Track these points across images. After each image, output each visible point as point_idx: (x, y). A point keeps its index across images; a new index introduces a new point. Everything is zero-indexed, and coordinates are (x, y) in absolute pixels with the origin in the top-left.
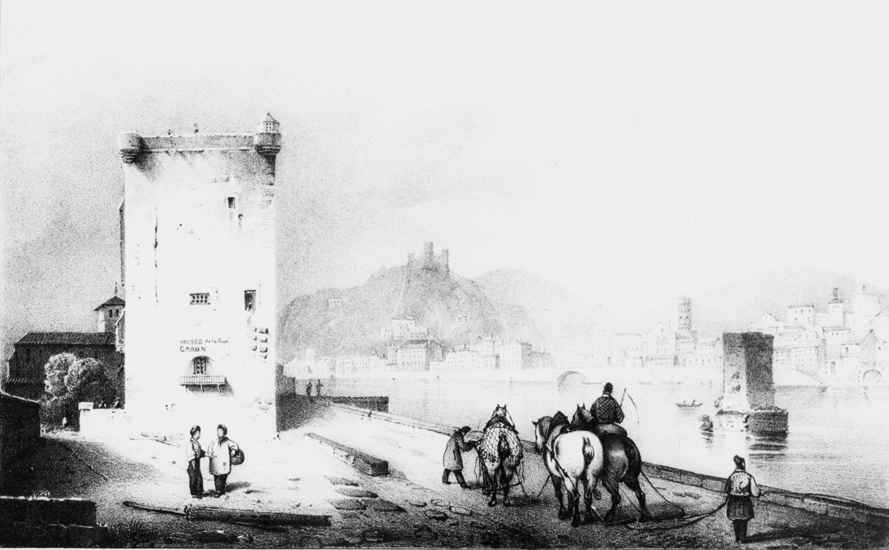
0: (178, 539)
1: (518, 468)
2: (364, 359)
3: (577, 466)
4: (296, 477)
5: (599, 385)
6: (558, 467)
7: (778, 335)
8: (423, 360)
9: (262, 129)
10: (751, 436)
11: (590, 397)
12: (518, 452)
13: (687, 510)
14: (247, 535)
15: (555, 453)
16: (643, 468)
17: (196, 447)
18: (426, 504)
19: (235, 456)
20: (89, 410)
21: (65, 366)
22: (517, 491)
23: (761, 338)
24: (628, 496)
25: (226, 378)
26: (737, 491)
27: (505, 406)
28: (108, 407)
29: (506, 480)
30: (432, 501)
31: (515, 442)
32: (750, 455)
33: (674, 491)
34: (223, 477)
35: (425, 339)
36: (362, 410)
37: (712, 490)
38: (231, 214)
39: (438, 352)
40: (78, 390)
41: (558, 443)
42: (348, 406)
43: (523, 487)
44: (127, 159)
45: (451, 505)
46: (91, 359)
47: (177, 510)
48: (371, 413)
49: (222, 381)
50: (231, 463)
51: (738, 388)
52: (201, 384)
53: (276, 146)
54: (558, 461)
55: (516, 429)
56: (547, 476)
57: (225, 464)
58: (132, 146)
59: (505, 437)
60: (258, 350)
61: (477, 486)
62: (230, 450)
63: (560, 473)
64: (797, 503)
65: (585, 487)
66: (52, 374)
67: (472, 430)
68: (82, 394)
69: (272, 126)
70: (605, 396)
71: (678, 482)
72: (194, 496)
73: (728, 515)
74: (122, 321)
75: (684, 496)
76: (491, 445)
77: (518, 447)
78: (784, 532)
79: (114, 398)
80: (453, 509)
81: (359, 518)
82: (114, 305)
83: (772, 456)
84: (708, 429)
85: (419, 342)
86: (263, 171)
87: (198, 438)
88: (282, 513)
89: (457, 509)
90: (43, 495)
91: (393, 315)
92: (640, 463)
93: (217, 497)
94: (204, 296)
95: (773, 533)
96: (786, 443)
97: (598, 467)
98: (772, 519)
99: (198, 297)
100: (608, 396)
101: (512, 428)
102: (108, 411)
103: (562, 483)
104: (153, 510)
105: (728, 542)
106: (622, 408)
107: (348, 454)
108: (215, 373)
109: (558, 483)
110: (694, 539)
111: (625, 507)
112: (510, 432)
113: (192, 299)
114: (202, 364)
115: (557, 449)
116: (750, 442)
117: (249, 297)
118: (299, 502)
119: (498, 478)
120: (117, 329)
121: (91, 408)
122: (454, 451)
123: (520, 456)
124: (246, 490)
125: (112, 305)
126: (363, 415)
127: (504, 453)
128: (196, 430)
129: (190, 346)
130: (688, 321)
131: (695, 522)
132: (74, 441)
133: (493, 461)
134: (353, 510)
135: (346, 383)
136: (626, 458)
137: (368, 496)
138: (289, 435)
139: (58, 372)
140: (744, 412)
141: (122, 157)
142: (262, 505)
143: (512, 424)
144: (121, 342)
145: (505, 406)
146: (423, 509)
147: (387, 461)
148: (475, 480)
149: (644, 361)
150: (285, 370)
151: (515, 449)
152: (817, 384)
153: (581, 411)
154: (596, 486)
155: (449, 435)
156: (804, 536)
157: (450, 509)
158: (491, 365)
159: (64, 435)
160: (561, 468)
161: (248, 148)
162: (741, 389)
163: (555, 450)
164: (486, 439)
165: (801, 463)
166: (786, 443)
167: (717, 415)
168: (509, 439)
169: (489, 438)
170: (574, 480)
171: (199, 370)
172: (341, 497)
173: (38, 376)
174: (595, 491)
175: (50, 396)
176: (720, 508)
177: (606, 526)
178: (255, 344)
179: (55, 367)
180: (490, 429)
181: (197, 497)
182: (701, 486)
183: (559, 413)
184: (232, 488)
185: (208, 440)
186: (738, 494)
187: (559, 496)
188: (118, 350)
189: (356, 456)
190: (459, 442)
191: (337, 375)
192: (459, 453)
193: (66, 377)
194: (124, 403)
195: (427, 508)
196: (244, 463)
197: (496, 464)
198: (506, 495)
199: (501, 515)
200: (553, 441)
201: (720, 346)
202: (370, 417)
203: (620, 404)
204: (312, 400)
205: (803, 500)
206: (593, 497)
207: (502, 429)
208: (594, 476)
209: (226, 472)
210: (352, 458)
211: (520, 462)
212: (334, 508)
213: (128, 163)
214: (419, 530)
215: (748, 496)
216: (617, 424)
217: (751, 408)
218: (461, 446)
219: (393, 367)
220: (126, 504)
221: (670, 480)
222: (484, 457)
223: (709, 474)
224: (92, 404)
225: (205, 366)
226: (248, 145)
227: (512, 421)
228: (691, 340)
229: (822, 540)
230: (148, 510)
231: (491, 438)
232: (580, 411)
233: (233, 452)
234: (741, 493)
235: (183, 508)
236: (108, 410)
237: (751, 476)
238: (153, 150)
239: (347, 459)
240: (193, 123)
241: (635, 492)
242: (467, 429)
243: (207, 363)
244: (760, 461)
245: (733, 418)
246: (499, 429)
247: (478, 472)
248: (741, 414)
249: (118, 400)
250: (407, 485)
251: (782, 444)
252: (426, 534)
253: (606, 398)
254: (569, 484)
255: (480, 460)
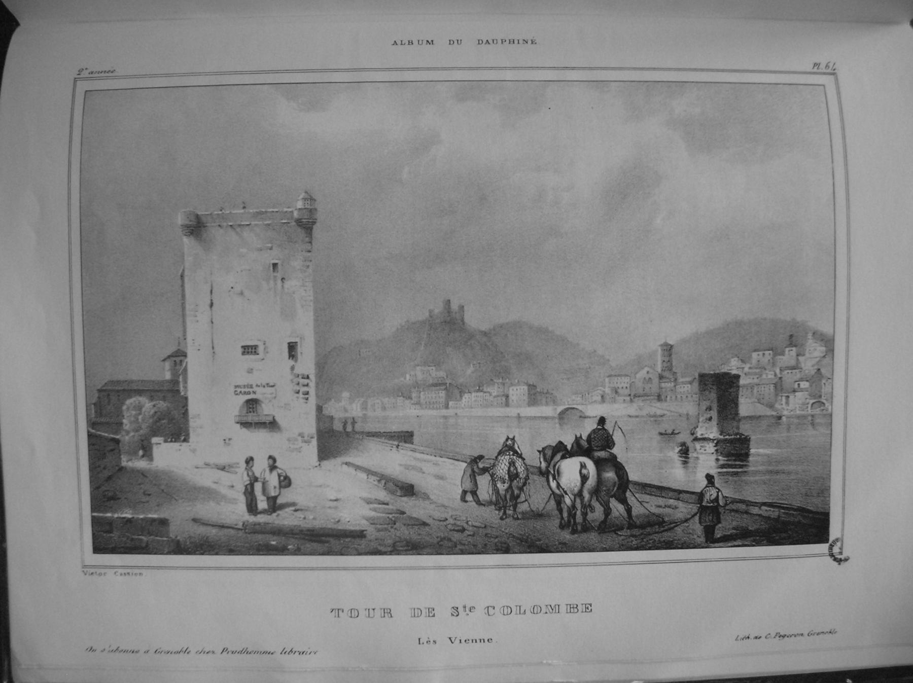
0: (238, 548)
1: (525, 488)
6: (559, 486)
7: (744, 375)
8: (443, 400)
12: (524, 476)
13: (666, 519)
14: (296, 545)
15: (557, 475)
17: (250, 474)
19: (283, 481)
20: (160, 444)
21: (139, 408)
22: (523, 507)
24: (617, 508)
27: (514, 437)
28: (175, 441)
30: (452, 516)
31: (522, 467)
32: (719, 473)
33: (656, 504)
34: (275, 498)
36: (391, 442)
37: (687, 502)
39: (456, 391)
42: (379, 440)
43: (529, 503)
44: (186, 233)
46: (161, 402)
48: (399, 445)
51: (710, 419)
55: (523, 456)
56: (549, 495)
57: (275, 487)
58: (191, 221)
61: (490, 503)
62: (279, 476)
63: (560, 491)
66: (128, 414)
67: (486, 457)
68: (155, 432)
69: (309, 202)
70: (599, 427)
71: (659, 497)
73: (700, 523)
74: (185, 370)
75: (664, 508)
76: (502, 469)
77: (525, 471)
79: (181, 434)
80: (470, 523)
81: (390, 532)
82: (178, 356)
83: (736, 474)
87: (252, 467)
89: (473, 522)
90: (126, 513)
93: (269, 515)
94: (254, 348)
95: (736, 535)
96: (748, 462)
98: (734, 524)
100: (601, 427)
101: (520, 456)
103: (562, 499)
105: (699, 542)
110: (672, 541)
111: (615, 518)
113: (243, 350)
114: (253, 405)
116: (720, 462)
119: (508, 497)
120: (181, 377)
121: (161, 442)
123: (527, 478)
124: (293, 508)
125: (176, 356)
126: (392, 447)
127: (513, 476)
129: (243, 390)
130: (669, 364)
131: (673, 528)
133: (504, 483)
134: (385, 525)
135: (377, 420)
136: (616, 478)
137: (398, 513)
138: (327, 464)
140: (715, 438)
141: (182, 231)
143: (520, 452)
144: (185, 388)
145: (514, 437)
146: (445, 523)
147: (413, 484)
148: (488, 499)
149: (632, 398)
153: (579, 440)
154: (591, 501)
155: (466, 462)
157: (467, 523)
158: (502, 403)
160: (561, 487)
161: (289, 221)
163: (556, 473)
164: (498, 465)
165: (760, 478)
166: (748, 462)
168: (517, 465)
169: (500, 464)
170: (572, 497)
171: (251, 410)
172: (373, 514)
174: (590, 506)
175: (128, 432)
176: (693, 516)
177: (599, 533)
180: (501, 457)
182: (678, 499)
184: (283, 507)
185: (260, 467)
186: (708, 505)
187: (560, 511)
188: (182, 394)
191: (370, 413)
192: (475, 476)
195: (448, 522)
197: (506, 485)
198: (515, 510)
200: (555, 466)
202: (398, 448)
203: (611, 433)
204: (348, 434)
205: (760, 508)
206: (588, 510)
207: (512, 456)
209: (276, 494)
210: (383, 482)
214: (441, 541)
216: (609, 450)
217: (721, 435)
220: (195, 520)
221: (653, 495)
222: (496, 480)
224: (162, 438)
225: (256, 406)
227: (520, 450)
230: (213, 526)
231: (502, 464)
232: (578, 440)
233: (282, 478)
234: (710, 503)
236: (176, 444)
239: (379, 483)
241: (624, 505)
242: (481, 457)
243: (258, 405)
246: (508, 456)
247: (491, 492)
248: (712, 439)
249: (184, 435)
250: (430, 503)
252: (446, 543)
253: (600, 429)
254: (568, 500)
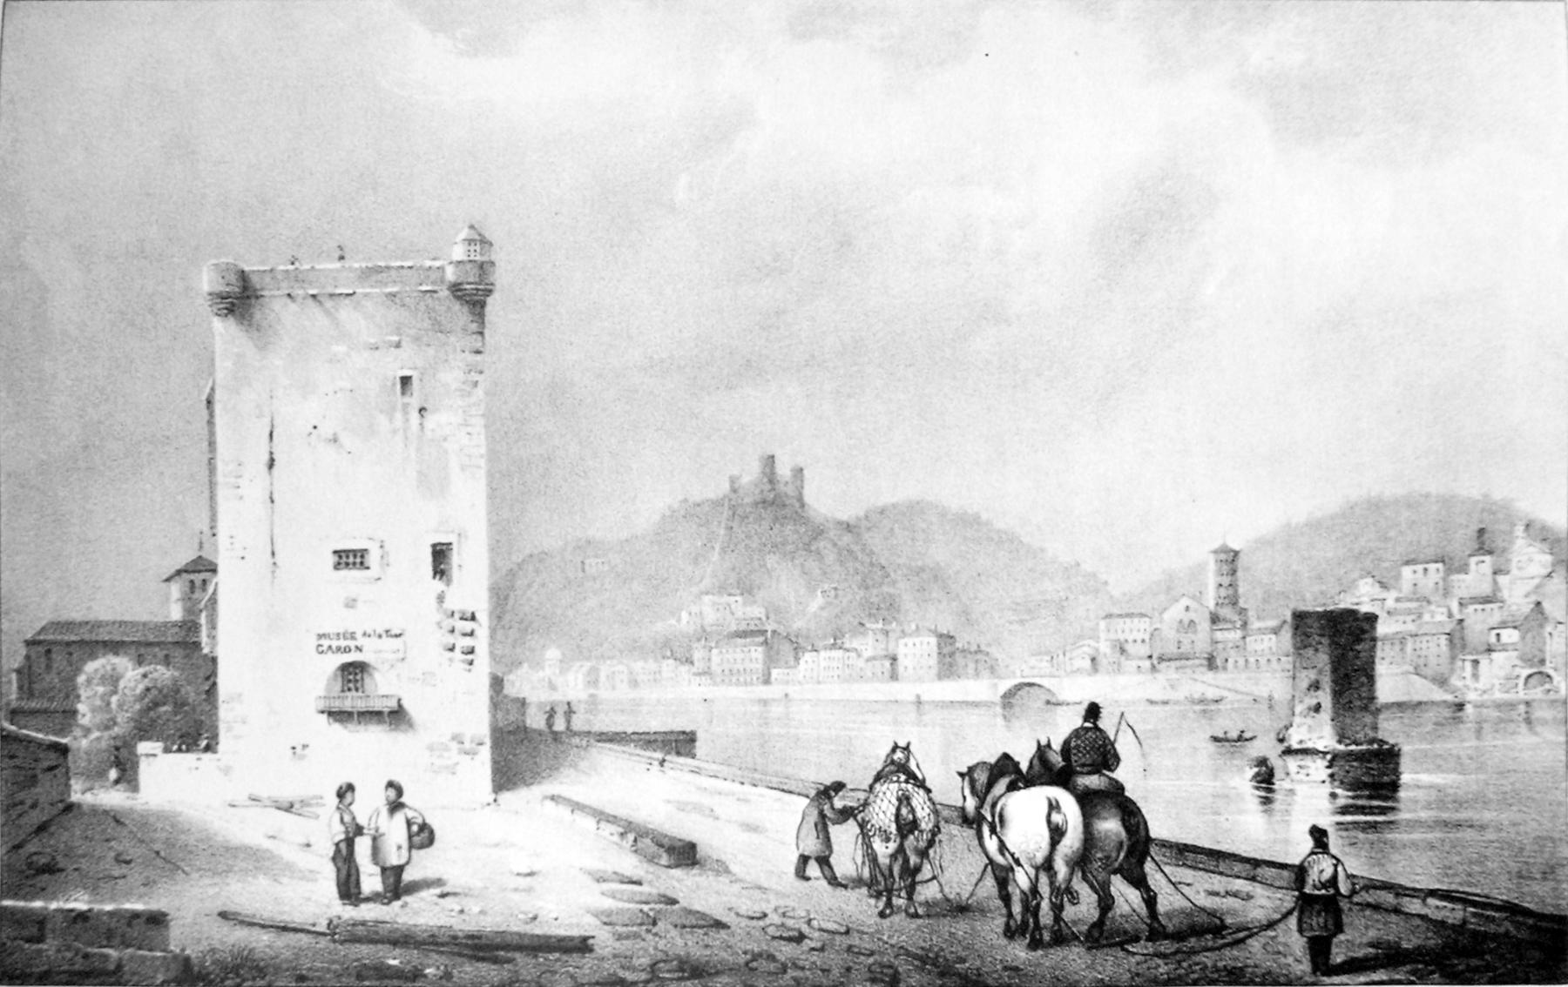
1: (931, 852)
2: (652, 665)
3: (1037, 846)
4: (528, 871)
5: (1077, 706)
6: (1002, 847)
7: (1385, 615)
8: (759, 666)
9: (459, 253)
10: (1339, 791)
11: (1061, 727)
12: (930, 826)
13: (1229, 921)
16: (1153, 850)
17: (347, 818)
18: (765, 915)
20: (154, 755)
21: (113, 680)
22: (928, 892)
23: (1357, 619)
24: (1126, 897)
25: (399, 700)
26: (1315, 886)
27: (909, 744)
28: (188, 751)
29: (911, 873)
34: (399, 870)
35: (760, 627)
36: (648, 754)
38: (405, 406)
39: (786, 648)
40: (136, 721)
41: (1002, 809)
43: (941, 885)
45: (812, 916)
46: (159, 667)
47: (314, 925)
48: (664, 761)
49: (393, 704)
50: (411, 847)
51: (1317, 708)
52: (355, 710)
53: (487, 284)
54: (1003, 838)
55: (928, 784)
57: (399, 847)
58: (228, 285)
59: (908, 799)
60: (458, 650)
61: (858, 882)
62: (409, 823)
63: (1006, 859)
64: (1414, 906)
65: (1052, 883)
66: (90, 693)
68: (144, 730)
72: (346, 902)
73: (1301, 931)
74: (213, 601)
75: (1224, 897)
76: (883, 812)
77: (932, 816)
78: (1389, 956)
80: (815, 923)
82: (199, 572)
83: (1373, 826)
84: (1266, 778)
85: (752, 633)
86: (464, 330)
87: (350, 804)
88: (503, 932)
90: (75, 900)
91: (702, 586)
92: (1148, 840)
94: (359, 554)
95: (1376, 957)
97: (1078, 849)
99: (348, 557)
101: (921, 784)
102: (190, 758)
103: (1011, 875)
104: (272, 927)
106: (1117, 746)
107: (621, 830)
108: (383, 687)
109: (1003, 878)
111: (1122, 916)
112: (916, 789)
113: (337, 559)
114: (356, 674)
115: (1001, 816)
117: (440, 554)
118: (535, 912)
120: (203, 615)
122: (816, 825)
123: (936, 830)
124: (438, 891)
125: (194, 572)
127: (907, 827)
128: (345, 792)
129: (335, 644)
131: (1242, 941)
132: (131, 809)
133: (888, 840)
136: (1123, 834)
137: (661, 902)
139: (101, 689)
141: (210, 306)
142: (467, 918)
143: (920, 777)
144: (213, 637)
145: (909, 744)
146: (761, 923)
147: (694, 841)
148: (854, 874)
149: (1155, 662)
150: (507, 685)
151: (927, 819)
152: (1449, 698)
155: (808, 797)
156: (1427, 964)
157: (809, 922)
159: (111, 797)
161: (436, 288)
162: (1321, 710)
163: (997, 819)
164: (874, 802)
167: (1280, 756)
168: (914, 803)
169: (878, 801)
170: (1032, 872)
171: (351, 685)
173: (67, 696)
178: (451, 640)
179: (95, 681)
181: (350, 904)
182: (1253, 879)
183: (1006, 756)
184: (414, 888)
185: (369, 805)
186: (1317, 892)
187: (1006, 898)
188: (206, 651)
189: (637, 833)
190: (826, 807)
193: (114, 699)
194: (217, 744)
195: (768, 921)
196: (436, 844)
197: (893, 846)
198: (910, 898)
199: (903, 931)
200: (994, 805)
201: (1287, 635)
202: (662, 766)
203: (1112, 738)
204: (556, 736)
206: (1066, 899)
207: (903, 785)
208: (1067, 863)
209: (402, 861)
210: (631, 837)
211: (935, 841)
212: (598, 923)
213: (219, 315)
215: (1334, 895)
217: (1340, 742)
218: (828, 815)
219: (703, 678)
220: (223, 915)
223: (1267, 858)
224: (160, 745)
226: (433, 283)
228: (1238, 624)
229: (1456, 969)
230: (263, 926)
232: (1042, 751)
233: (415, 828)
235: (325, 923)
237: (1338, 860)
238: (263, 293)
239: (622, 840)
240: (336, 244)
242: (839, 786)
244: (1353, 833)
245: (1308, 761)
246: (896, 785)
247: (859, 860)
249: (207, 738)
250: (731, 882)
251: (1394, 805)
253: (1088, 729)
254: (1022, 879)
255: (864, 838)
